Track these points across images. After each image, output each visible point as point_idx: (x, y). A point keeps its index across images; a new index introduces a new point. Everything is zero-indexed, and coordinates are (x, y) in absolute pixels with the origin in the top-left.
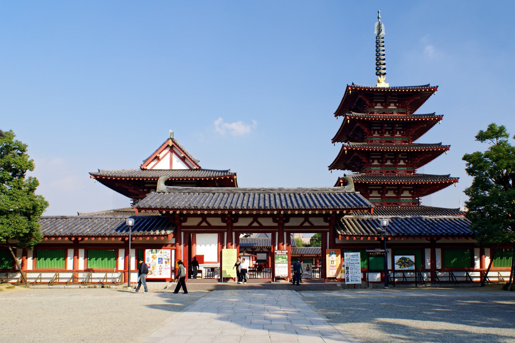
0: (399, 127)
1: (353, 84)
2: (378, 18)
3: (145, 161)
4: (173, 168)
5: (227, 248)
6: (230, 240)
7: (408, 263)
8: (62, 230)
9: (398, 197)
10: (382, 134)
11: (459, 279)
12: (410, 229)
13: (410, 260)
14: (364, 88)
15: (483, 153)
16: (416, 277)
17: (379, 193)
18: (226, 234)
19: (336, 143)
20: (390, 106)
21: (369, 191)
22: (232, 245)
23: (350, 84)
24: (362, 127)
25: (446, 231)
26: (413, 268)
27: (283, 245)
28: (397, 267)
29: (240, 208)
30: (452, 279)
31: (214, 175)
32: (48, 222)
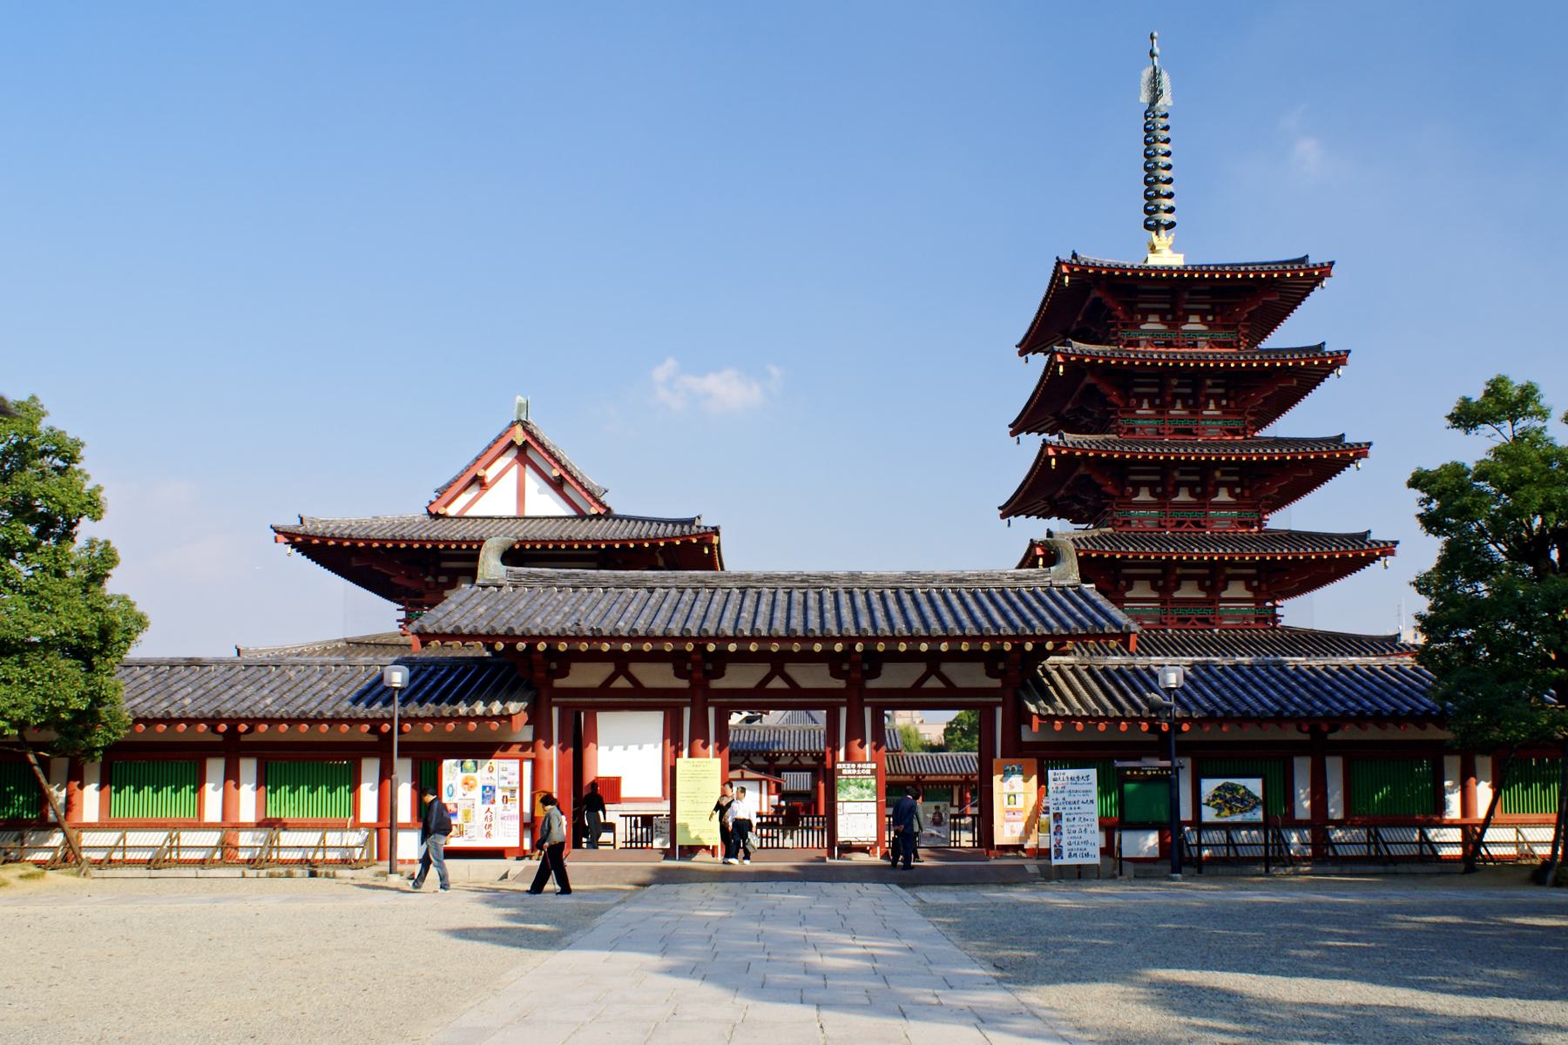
0: (1215, 386)
1: (1074, 256)
2: (1152, 55)
3: (441, 492)
4: (528, 513)
5: (691, 755)
6: (699, 731)
7: (1242, 801)
8: (188, 701)
9: (1213, 600)
10: (1162, 409)
11: (1396, 851)
12: (1249, 699)
13: (1248, 793)
14: (1109, 267)
15: (1471, 465)
16: (1266, 845)
17: (1154, 588)
18: (687, 712)
19: (1023, 435)
20: (1186, 322)
21: (1123, 583)
22: (705, 746)
23: (1067, 257)
24: (1103, 388)
25: (1359, 703)
26: (1258, 815)
27: (862, 745)
28: (1209, 814)
29: (730, 633)
30: (1378, 849)
31: (652, 534)
32: (147, 678)
